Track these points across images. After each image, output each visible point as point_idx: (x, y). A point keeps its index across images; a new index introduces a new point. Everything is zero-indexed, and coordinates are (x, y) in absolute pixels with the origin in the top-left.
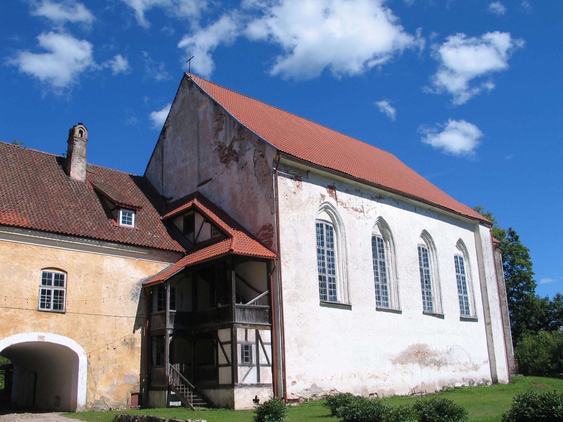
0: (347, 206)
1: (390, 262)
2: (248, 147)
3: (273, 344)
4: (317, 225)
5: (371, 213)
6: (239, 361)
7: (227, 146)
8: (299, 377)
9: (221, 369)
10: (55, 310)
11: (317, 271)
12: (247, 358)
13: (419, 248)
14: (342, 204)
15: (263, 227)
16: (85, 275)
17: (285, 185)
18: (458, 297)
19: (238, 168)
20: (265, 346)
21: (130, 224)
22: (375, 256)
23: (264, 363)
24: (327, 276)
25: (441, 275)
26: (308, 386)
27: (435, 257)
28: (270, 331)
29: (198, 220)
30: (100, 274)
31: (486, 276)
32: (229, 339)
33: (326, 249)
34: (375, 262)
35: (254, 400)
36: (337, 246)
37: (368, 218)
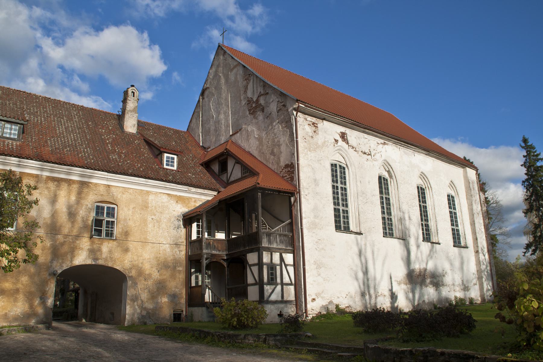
0: (357, 149)
1: (394, 197)
2: (272, 100)
3: (295, 265)
4: (332, 165)
5: (378, 156)
7: (255, 100)
8: (318, 295)
9: (250, 289)
10: (107, 238)
11: (333, 204)
12: (272, 280)
13: (418, 187)
14: (353, 148)
15: (286, 165)
16: (133, 208)
17: (303, 124)
18: (451, 230)
19: (264, 119)
20: (288, 267)
21: (173, 166)
22: (381, 192)
23: (287, 282)
24: (341, 208)
25: (436, 211)
26: (325, 303)
27: (431, 195)
28: (292, 255)
29: (231, 164)
30: (146, 207)
31: (474, 212)
32: (256, 261)
33: (339, 185)
34: (382, 198)
35: (278, 315)
36: (349, 183)
37: (374, 161)
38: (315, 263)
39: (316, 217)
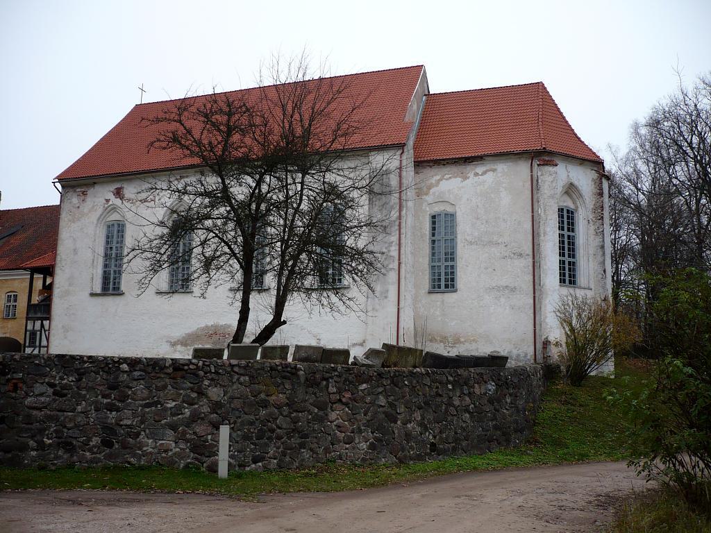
6: (27, 344)
38: (63, 327)
39: (70, 285)
